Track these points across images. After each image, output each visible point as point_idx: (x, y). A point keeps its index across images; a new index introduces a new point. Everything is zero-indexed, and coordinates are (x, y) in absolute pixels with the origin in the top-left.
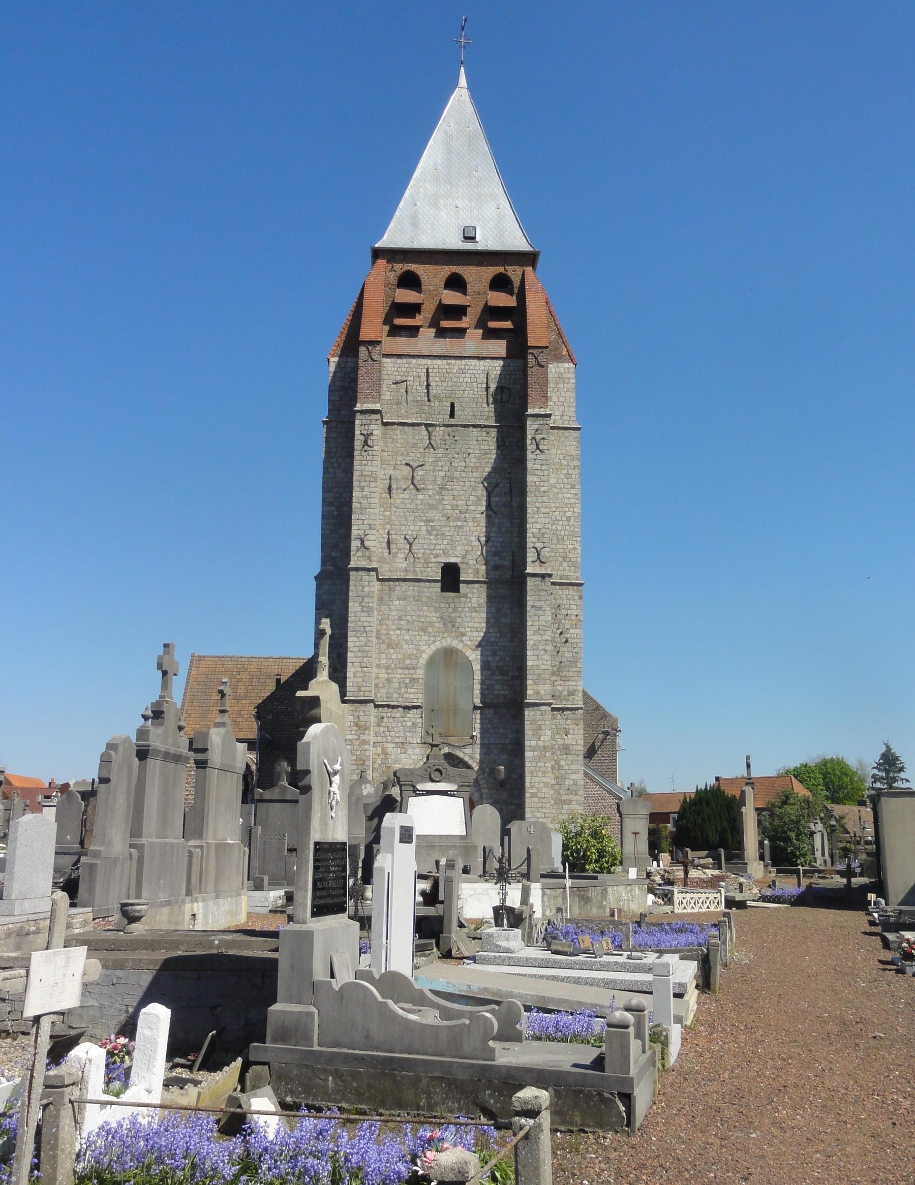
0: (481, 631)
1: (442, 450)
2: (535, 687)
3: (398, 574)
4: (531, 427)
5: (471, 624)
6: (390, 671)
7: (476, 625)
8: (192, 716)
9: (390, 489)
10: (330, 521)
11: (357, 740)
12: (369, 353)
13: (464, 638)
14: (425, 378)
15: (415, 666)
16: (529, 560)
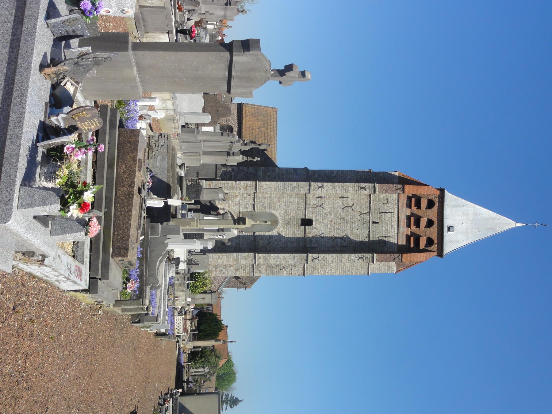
0: (285, 235)
2: (262, 257)
4: (369, 255)
6: (269, 198)
9: (343, 197)
11: (241, 186)
12: (399, 189)
13: (282, 228)
14: (389, 211)
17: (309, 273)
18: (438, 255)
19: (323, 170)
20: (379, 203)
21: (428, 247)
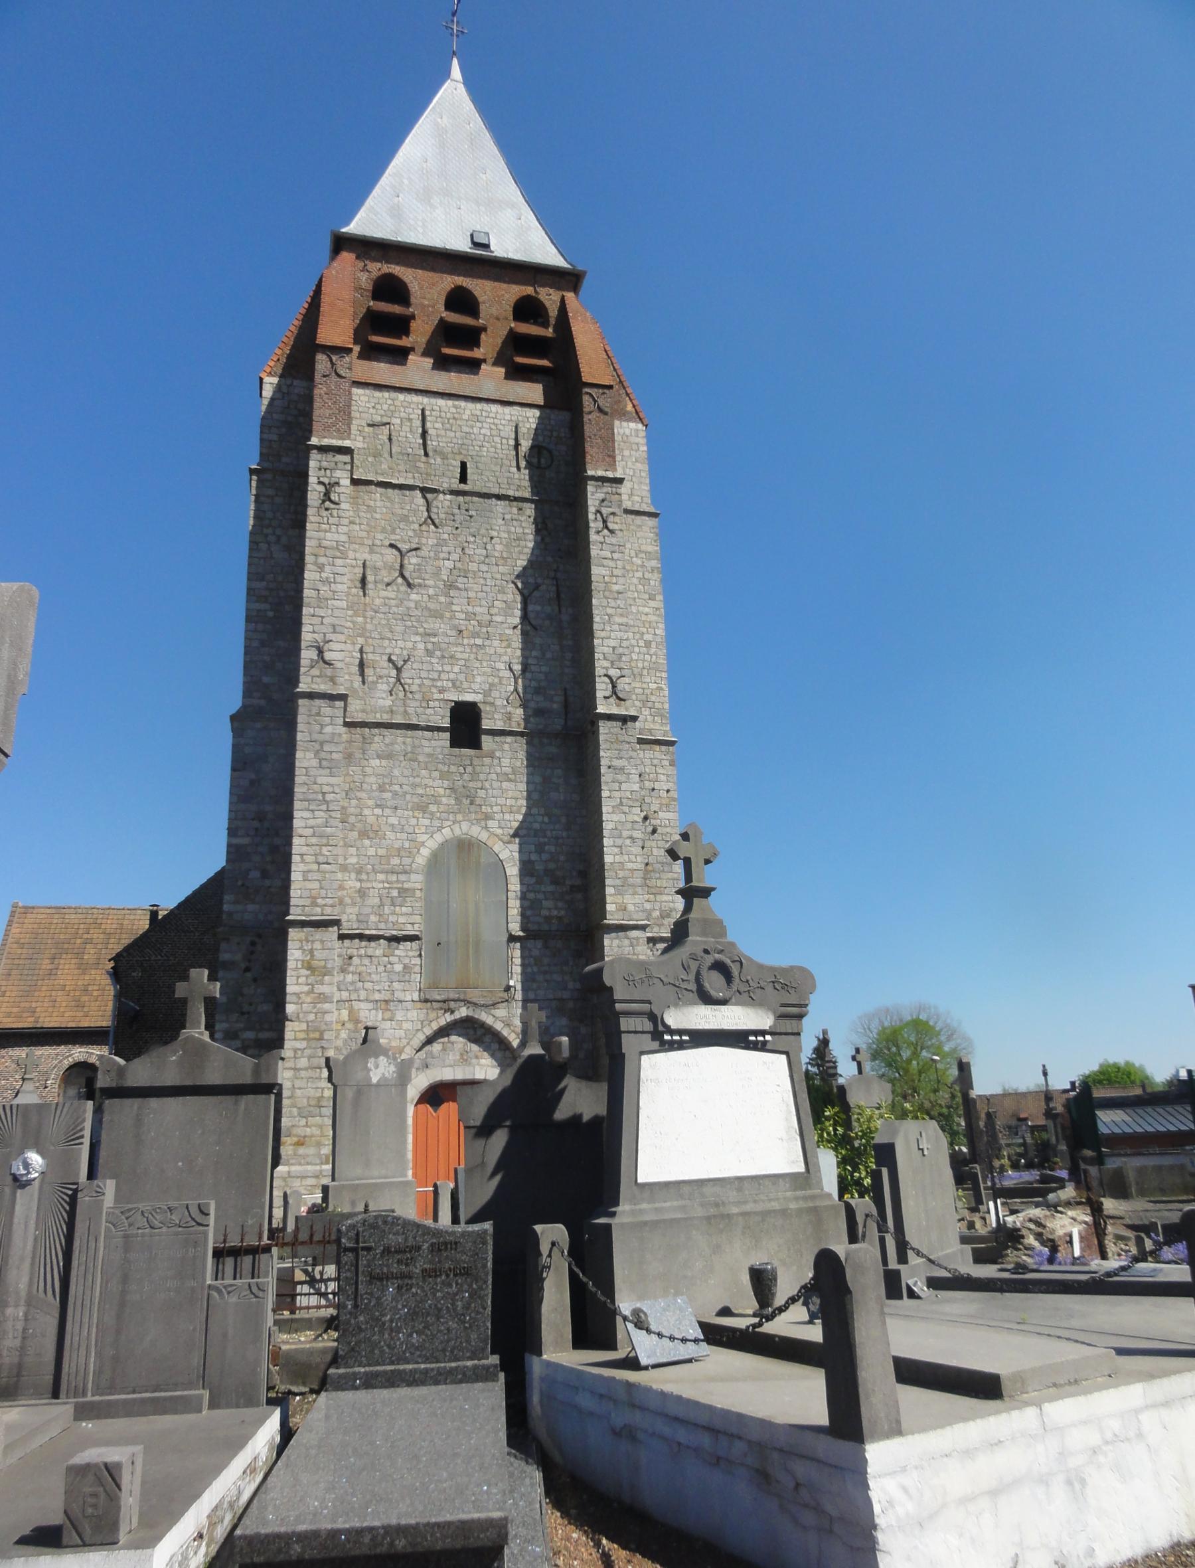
0: (518, 812)
1: (448, 529)
2: (619, 899)
3: (378, 716)
4: (594, 495)
5: (501, 801)
6: (364, 877)
7: (509, 802)
8: (8, 994)
9: (363, 581)
10: (260, 627)
11: (308, 993)
13: (490, 823)
14: (418, 423)
15: (408, 868)
16: (599, 694)
17: (662, 724)
18: (575, 288)
19: (246, 654)
20: (386, 455)
21: (548, 321)
